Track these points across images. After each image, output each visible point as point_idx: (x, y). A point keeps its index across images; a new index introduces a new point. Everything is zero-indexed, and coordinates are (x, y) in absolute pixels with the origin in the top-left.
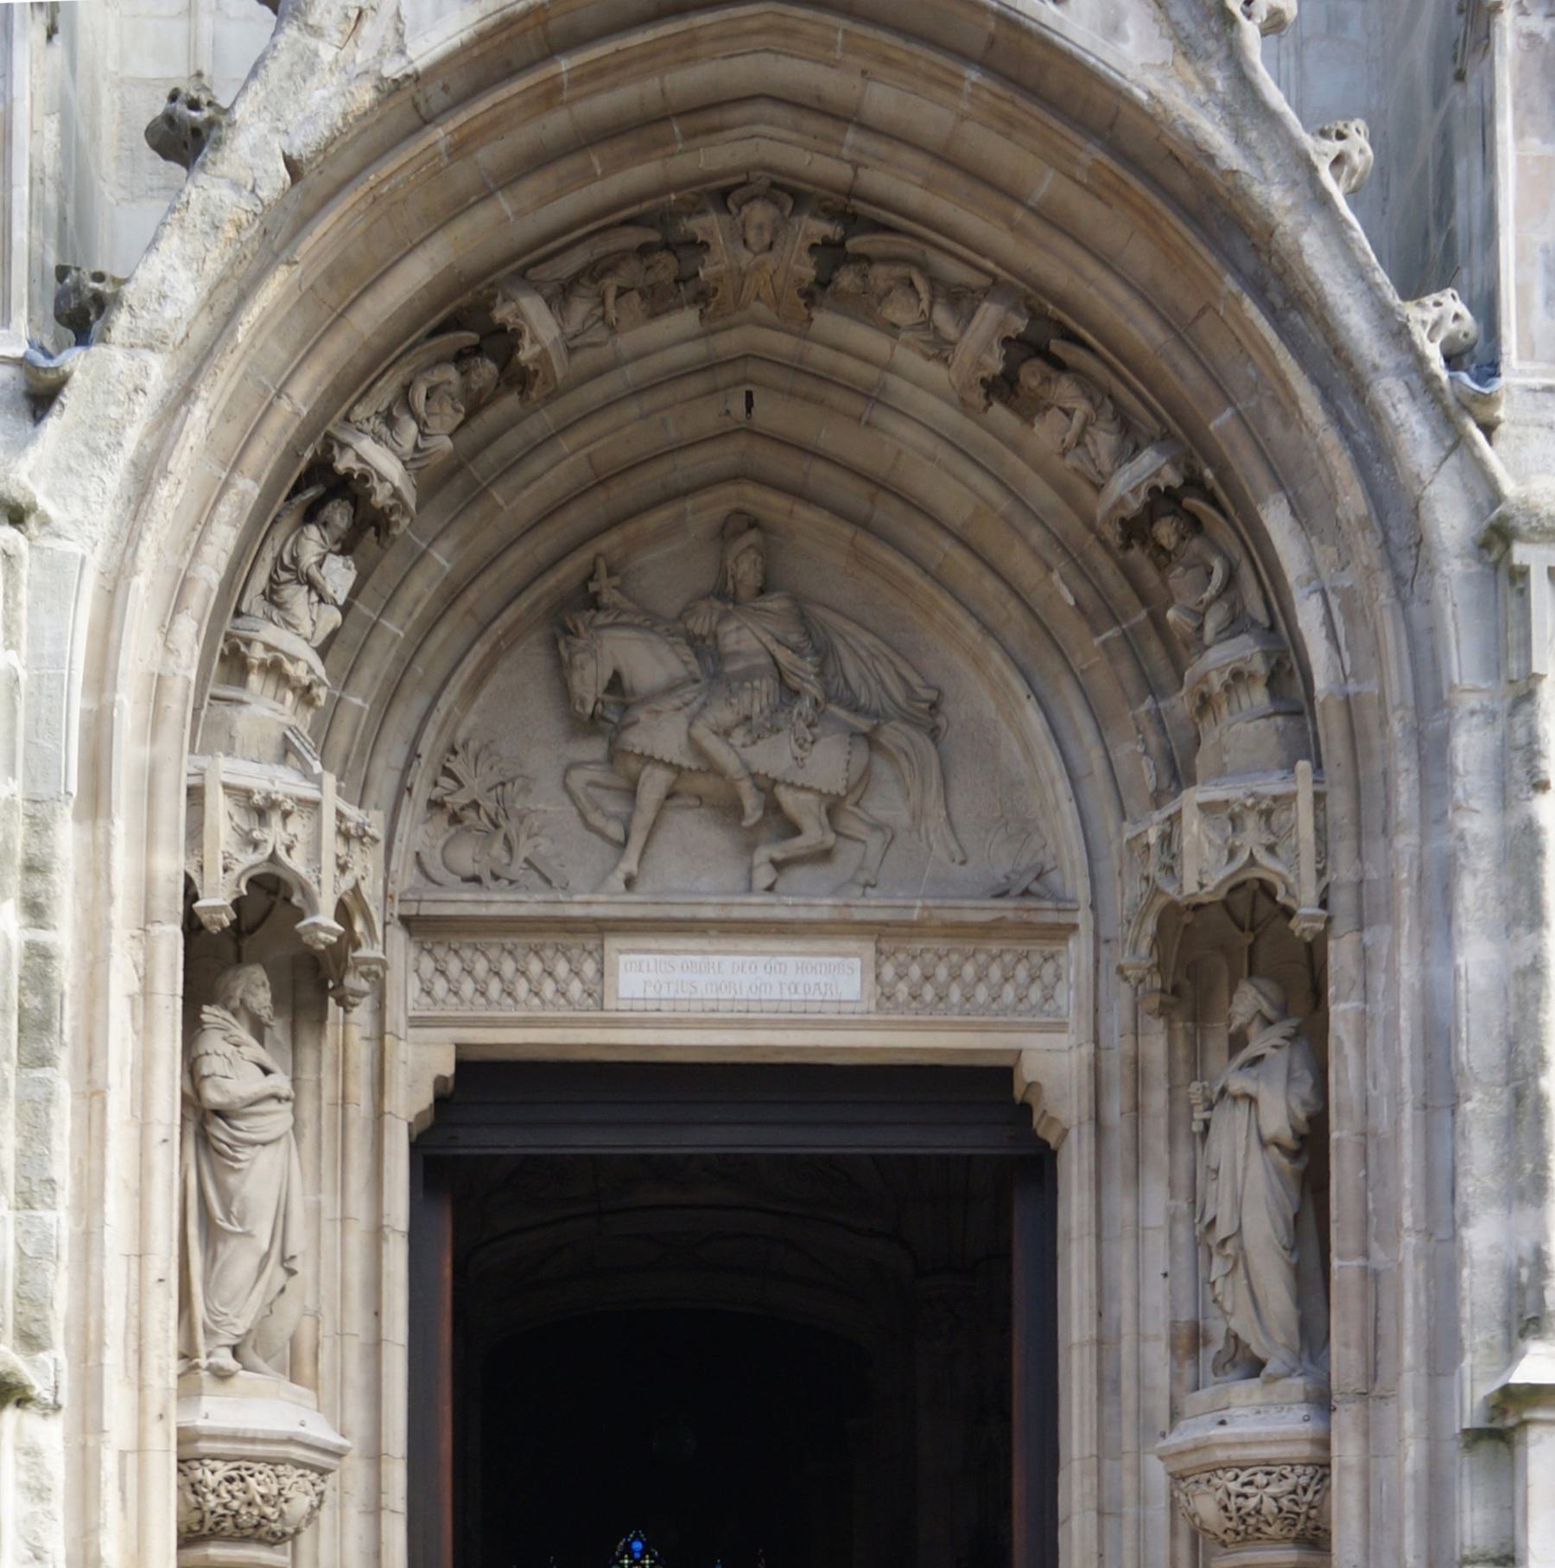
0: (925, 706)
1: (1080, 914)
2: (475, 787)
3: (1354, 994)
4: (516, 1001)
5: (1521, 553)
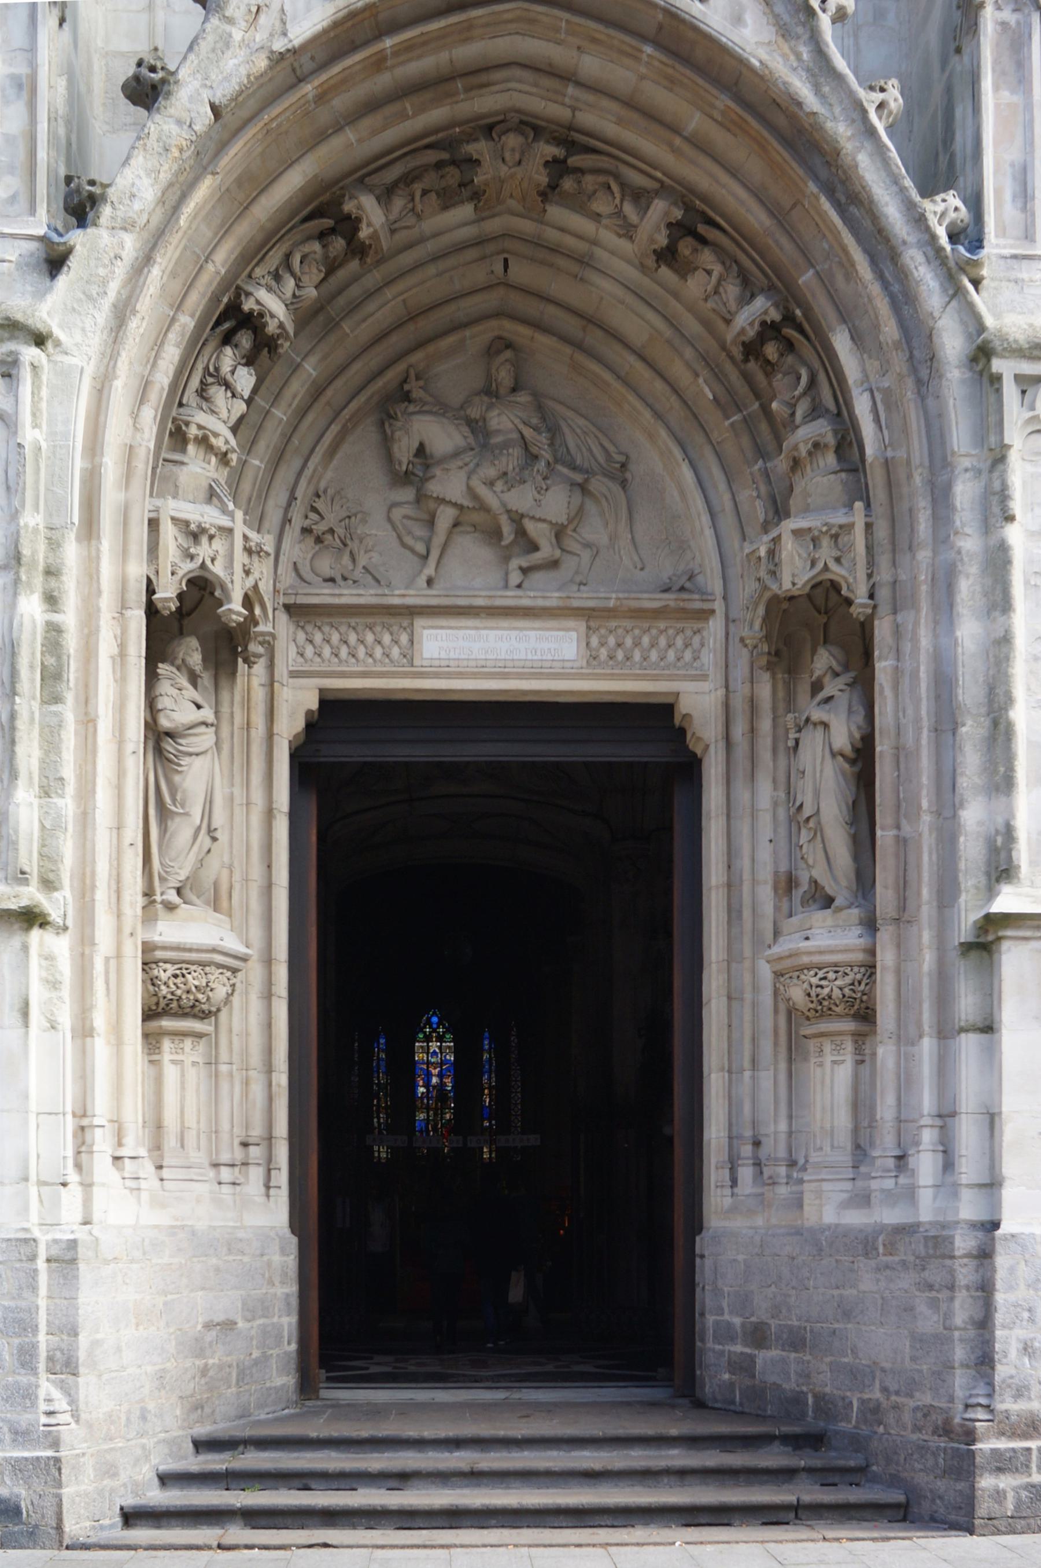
0: (618, 466)
1: (716, 603)
2: (331, 519)
4: (357, 660)
5: (998, 365)
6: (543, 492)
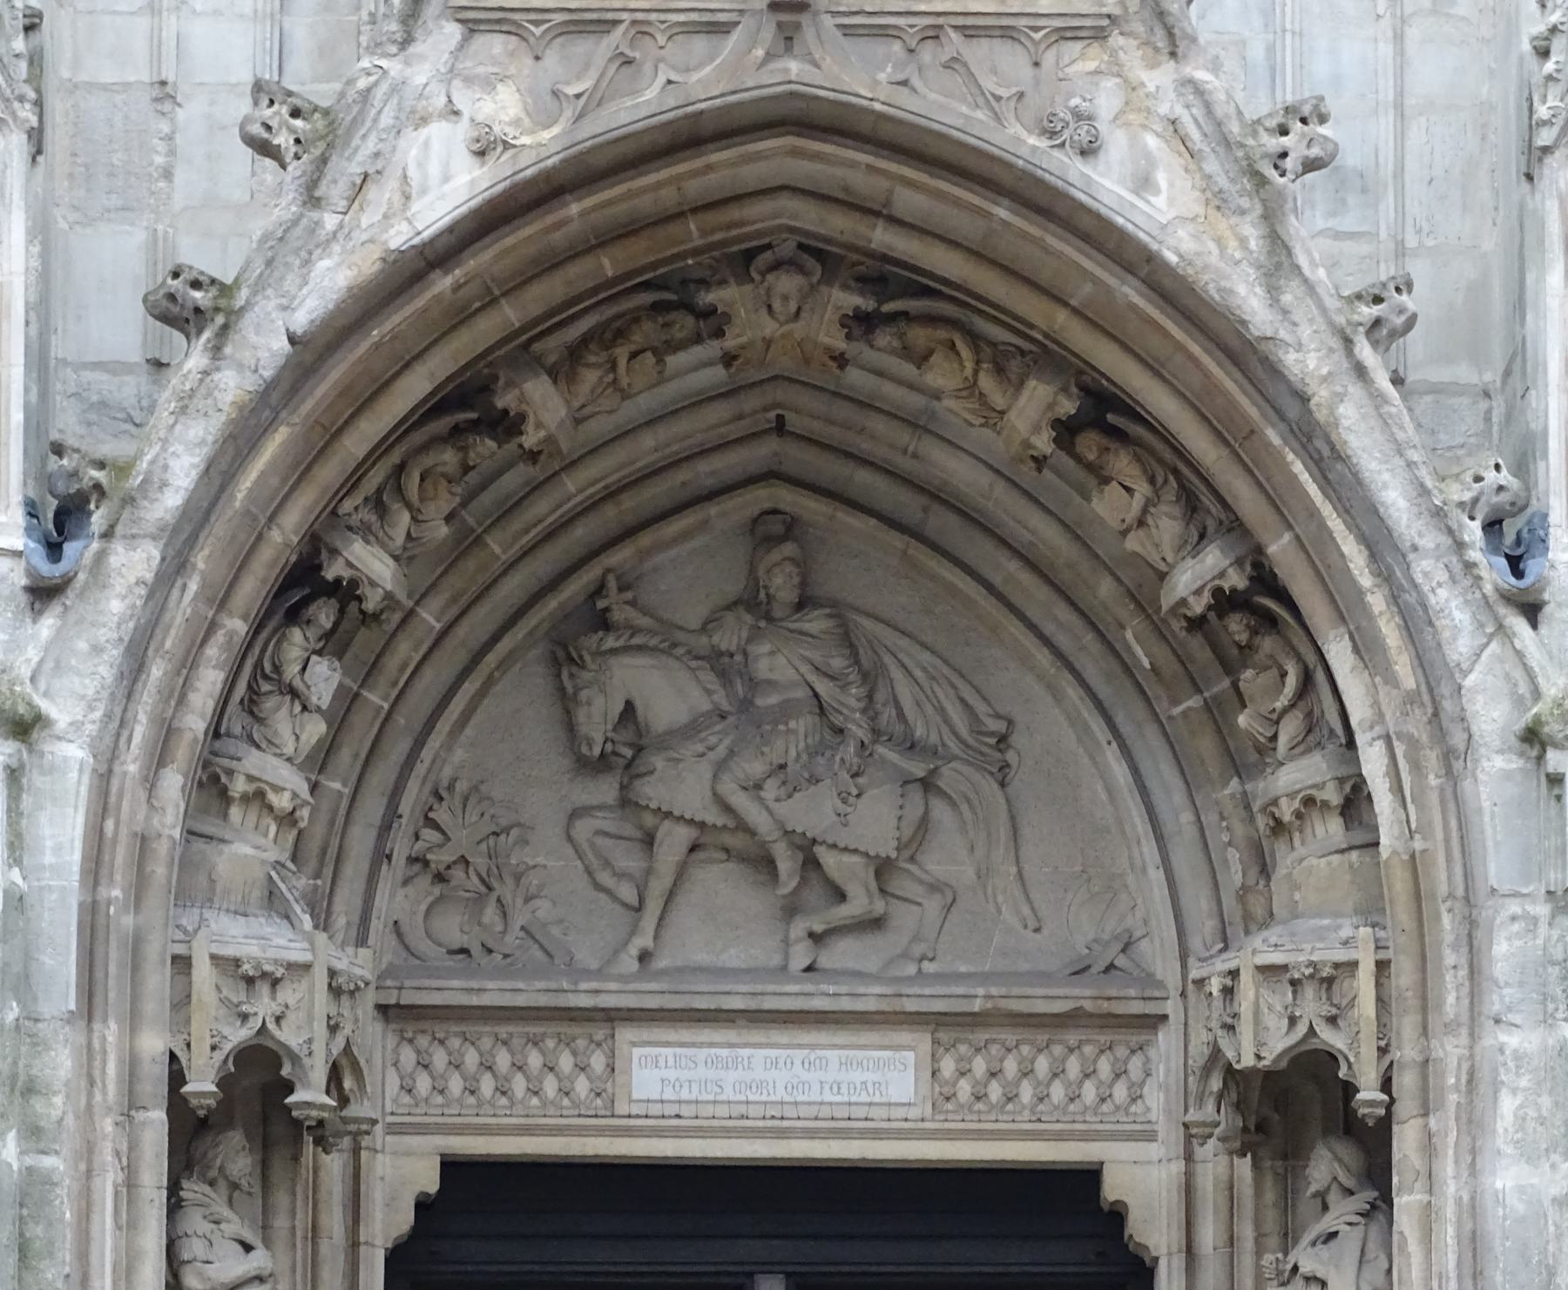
0: (993, 741)
1: (1169, 1002)
3: (1418, 1185)
4: (511, 1099)
6: (852, 800)
